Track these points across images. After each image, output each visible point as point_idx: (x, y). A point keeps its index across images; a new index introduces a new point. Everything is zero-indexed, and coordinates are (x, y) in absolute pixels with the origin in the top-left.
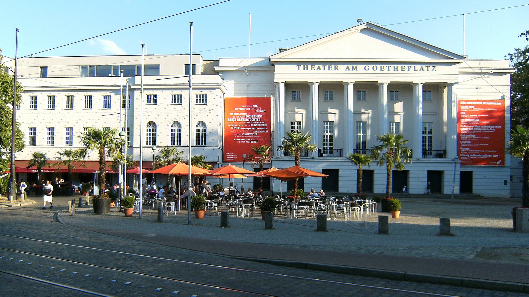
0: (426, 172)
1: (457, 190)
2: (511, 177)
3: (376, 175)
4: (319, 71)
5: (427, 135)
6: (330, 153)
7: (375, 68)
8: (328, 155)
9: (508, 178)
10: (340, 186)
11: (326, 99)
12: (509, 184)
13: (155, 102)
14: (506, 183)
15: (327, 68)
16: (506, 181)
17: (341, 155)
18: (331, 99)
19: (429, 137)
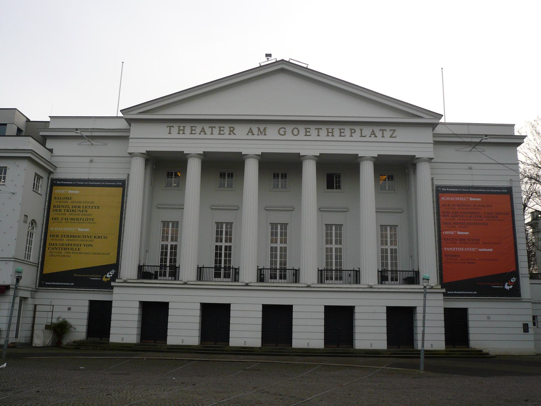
1: (317, 341)
2: (534, 318)
4: (202, 136)
6: (281, 278)
7: (296, 132)
9: (529, 320)
12: (531, 331)
14: (526, 328)
16: (527, 324)
17: (357, 280)
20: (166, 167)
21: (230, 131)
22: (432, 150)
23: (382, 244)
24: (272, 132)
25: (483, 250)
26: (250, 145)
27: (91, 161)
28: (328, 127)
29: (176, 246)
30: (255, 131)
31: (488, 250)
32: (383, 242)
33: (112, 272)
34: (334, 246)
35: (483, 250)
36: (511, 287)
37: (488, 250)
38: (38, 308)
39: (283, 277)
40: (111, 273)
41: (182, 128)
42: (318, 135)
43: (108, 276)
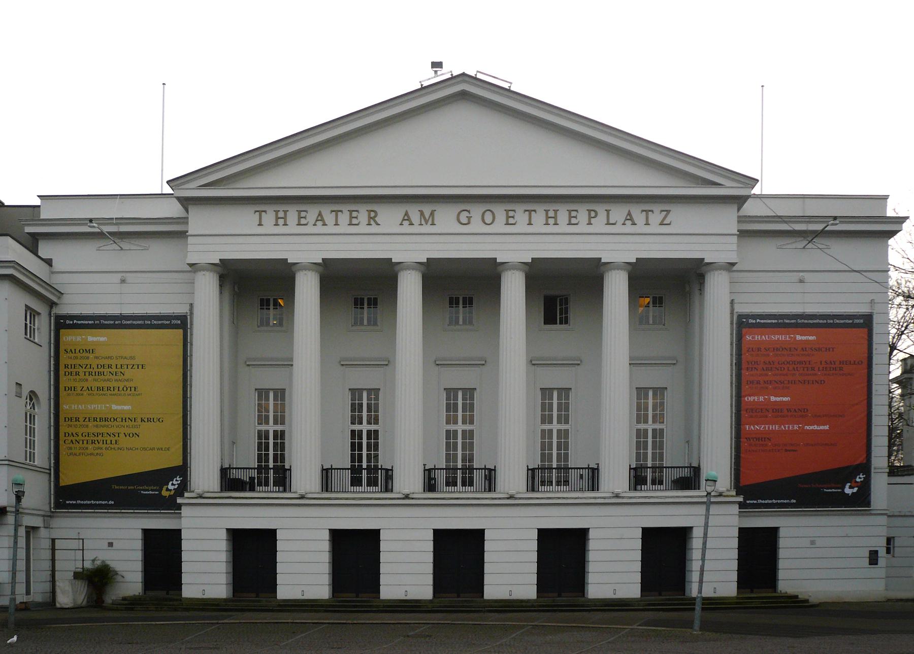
0: (639, 533)
2: (889, 540)
3: (593, 544)
4: (320, 228)
6: (464, 484)
7: (488, 218)
9: (880, 544)
10: (383, 580)
12: (882, 562)
14: (873, 558)
16: (876, 552)
17: (388, 489)
19: (464, 432)
20: (257, 289)
21: (370, 218)
22: (735, 247)
24: (446, 218)
25: (812, 428)
26: (406, 244)
27: (123, 281)
28: (277, 208)
29: (283, 433)
30: (415, 217)
31: (822, 428)
32: (546, 419)
33: (177, 481)
34: (555, 426)
35: (812, 428)
36: (855, 490)
37: (822, 428)
38: (58, 544)
40: (175, 482)
41: (281, 214)
42: (530, 224)
43: (170, 487)
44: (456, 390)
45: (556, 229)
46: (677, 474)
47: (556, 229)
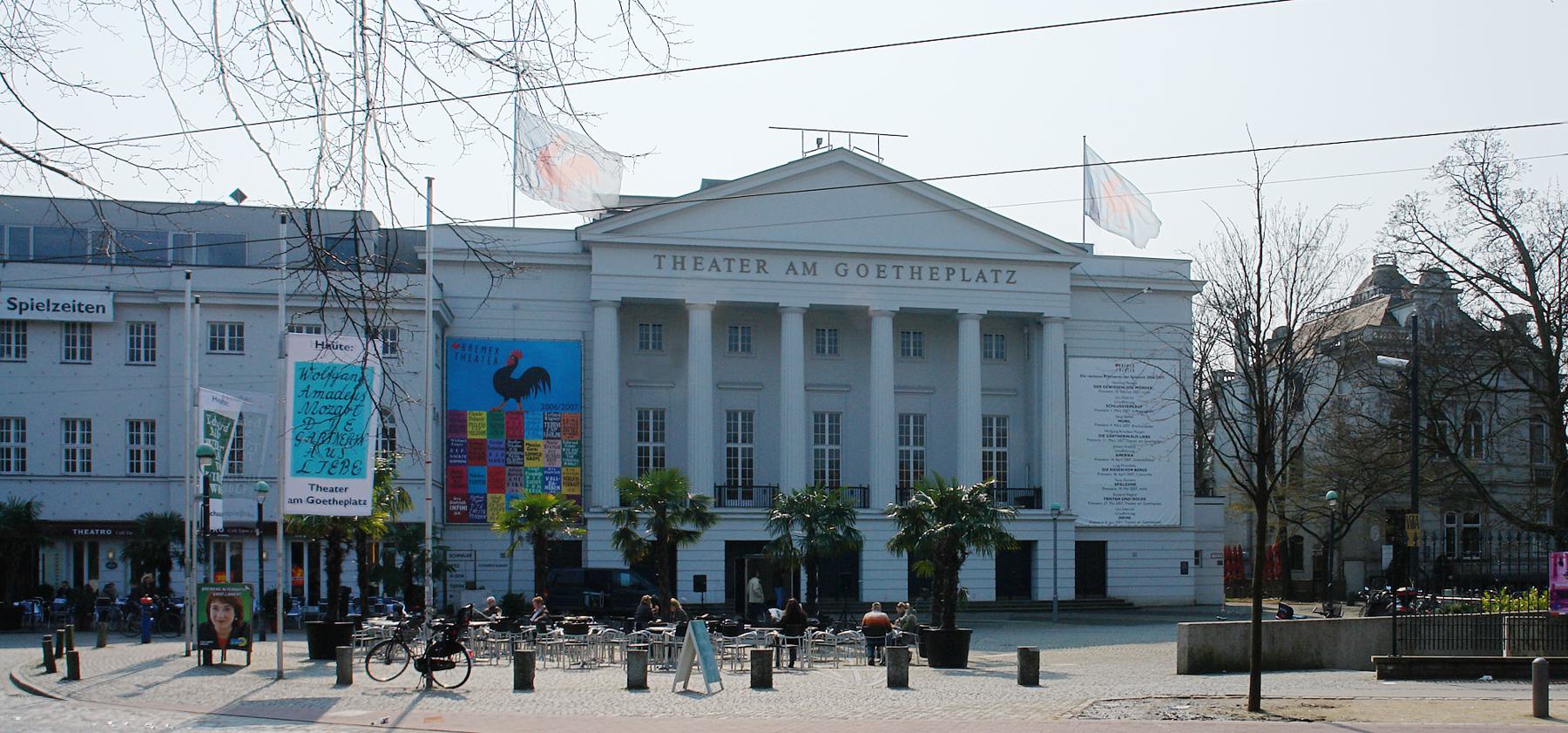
1: (1068, 591)
2: (1197, 553)
5: (912, 448)
7: (841, 270)
8: (740, 501)
9: (1189, 557)
11: (821, 351)
12: (1191, 572)
13: (238, 345)
14: (1184, 569)
15: (1003, 277)
18: (833, 351)
20: (652, 323)
23: (901, 444)
27: (515, 308)
29: (901, 444)
32: (819, 440)
34: (827, 447)
39: (748, 495)
44: (74, 422)
45: (920, 283)
46: (1022, 494)
47: (920, 283)
